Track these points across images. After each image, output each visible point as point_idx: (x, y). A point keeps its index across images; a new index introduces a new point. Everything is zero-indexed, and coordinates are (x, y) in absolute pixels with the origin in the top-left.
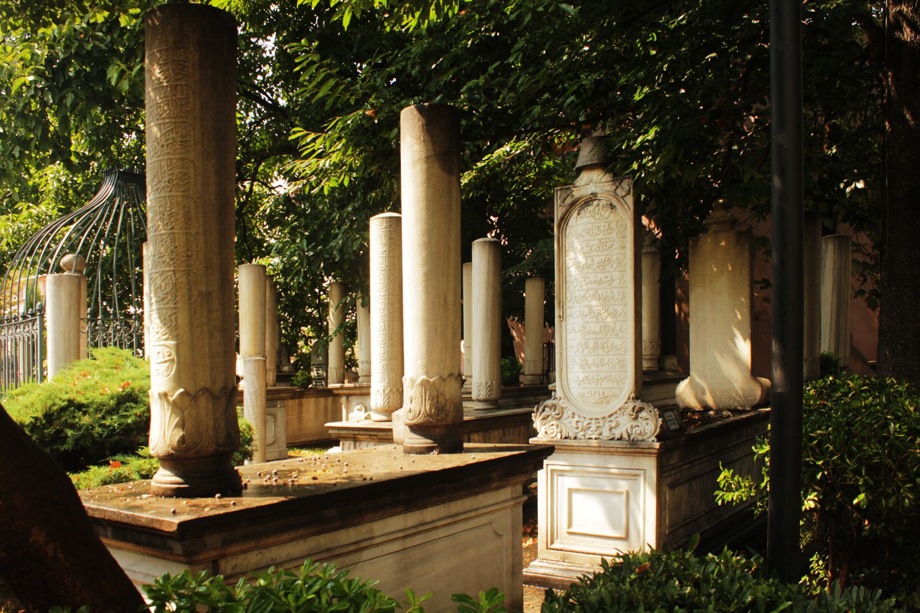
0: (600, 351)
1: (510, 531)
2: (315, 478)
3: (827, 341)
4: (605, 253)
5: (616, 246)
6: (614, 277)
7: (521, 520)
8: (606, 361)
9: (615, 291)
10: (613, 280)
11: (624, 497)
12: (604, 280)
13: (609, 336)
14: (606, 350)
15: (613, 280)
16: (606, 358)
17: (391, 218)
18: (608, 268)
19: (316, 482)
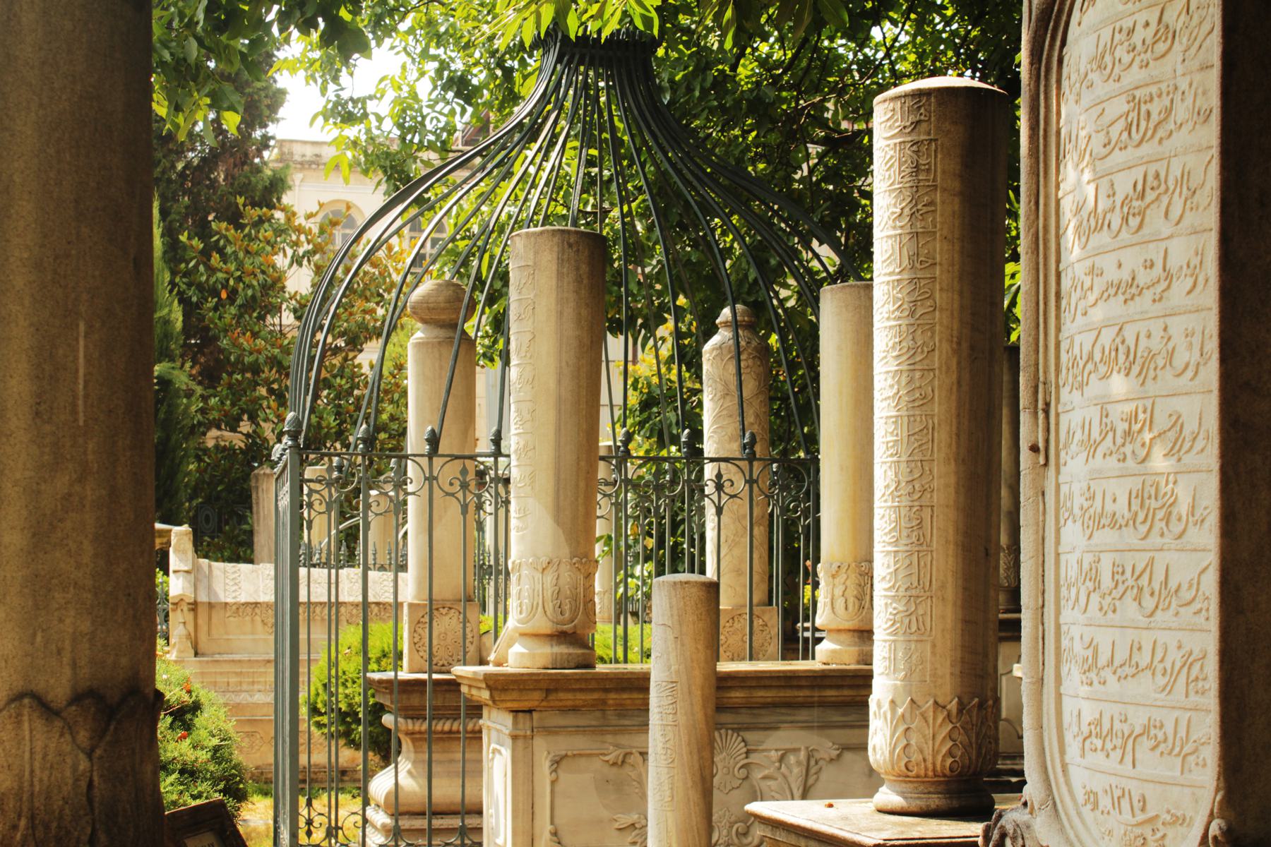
0: (1129, 609)
1: (252, 600)
2: (831, 806)
3: (650, 779)
4: (1146, 149)
5: (1181, 112)
6: (1175, 262)
7: (250, 566)
8: (1144, 658)
9: (1178, 326)
10: (1169, 277)
11: (1169, 320)
12: (1143, 278)
13: (1155, 540)
14: (1149, 603)
15: (1169, 277)
16: (1146, 639)
17: (919, 94)
18: (1156, 223)
19: (828, 802)
